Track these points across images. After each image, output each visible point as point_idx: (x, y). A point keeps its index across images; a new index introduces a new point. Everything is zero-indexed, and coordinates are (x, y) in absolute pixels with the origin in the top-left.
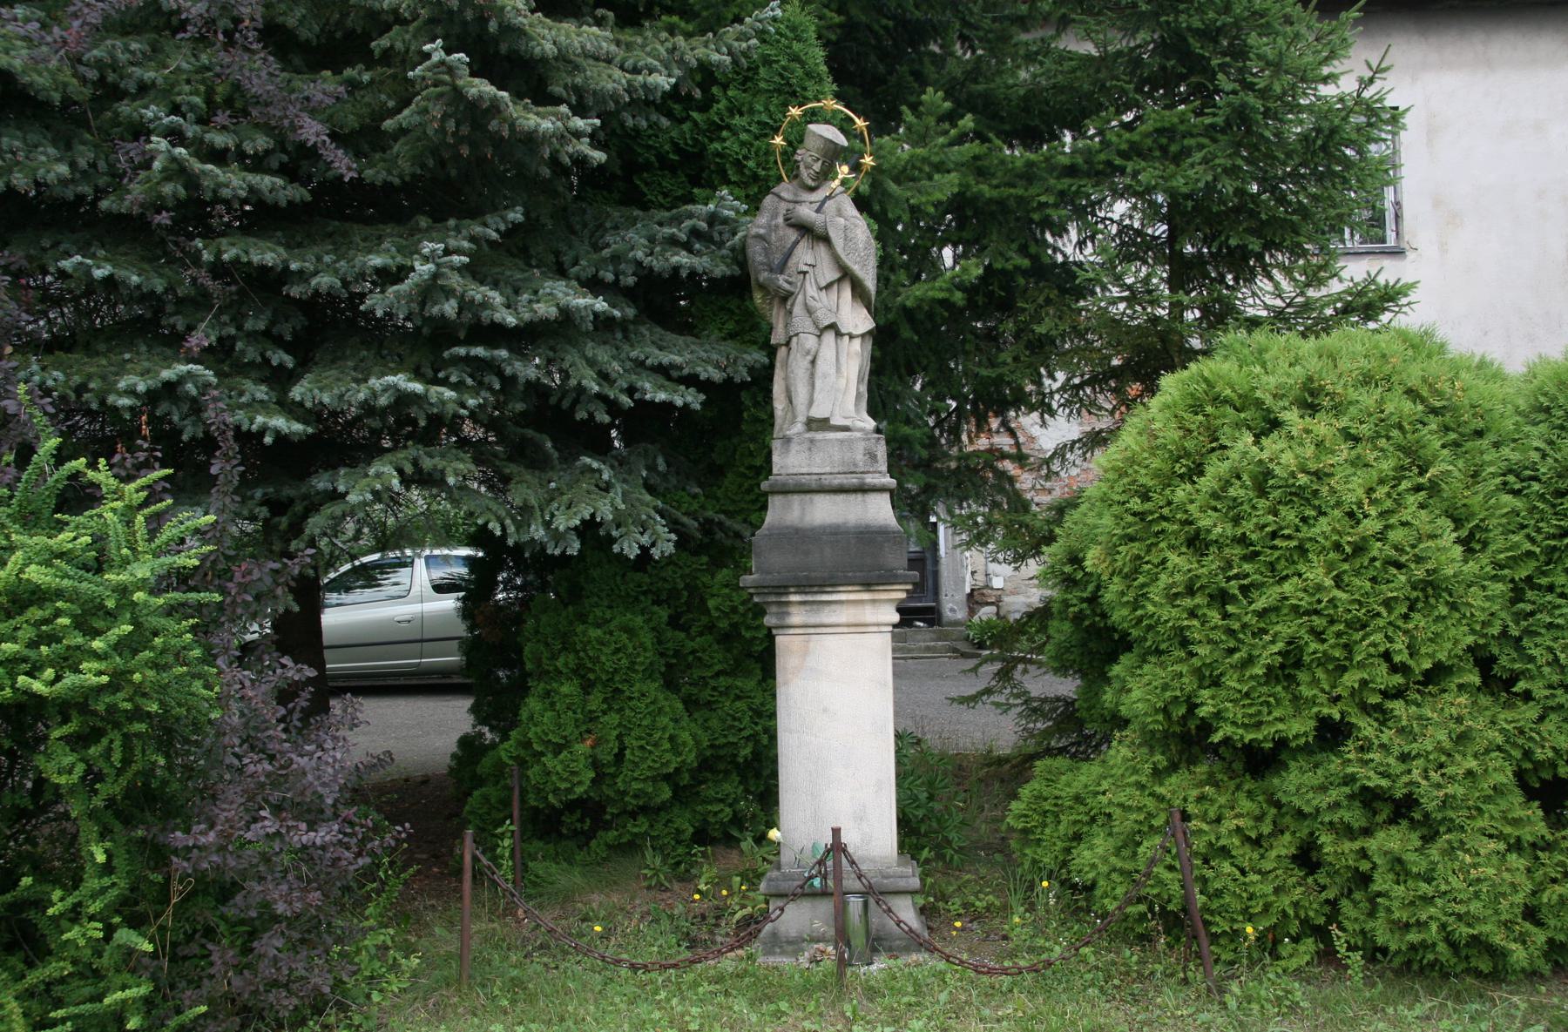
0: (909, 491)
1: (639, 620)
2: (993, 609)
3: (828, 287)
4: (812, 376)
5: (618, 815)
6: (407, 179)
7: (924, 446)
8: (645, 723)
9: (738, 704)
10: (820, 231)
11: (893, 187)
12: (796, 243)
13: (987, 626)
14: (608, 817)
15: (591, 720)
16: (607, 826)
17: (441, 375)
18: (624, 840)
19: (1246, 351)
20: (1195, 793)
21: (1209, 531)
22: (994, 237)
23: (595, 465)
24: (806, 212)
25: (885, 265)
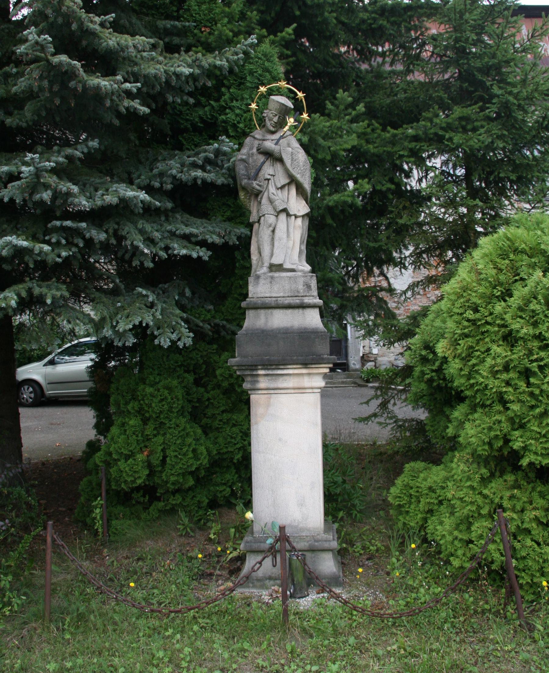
0: (332, 308)
1: (175, 382)
2: (373, 363)
3: (282, 187)
4: (273, 239)
5: (165, 493)
6: (31, 123)
7: (340, 284)
8: (178, 442)
9: (234, 429)
10: (277, 155)
11: (321, 141)
12: (264, 163)
13: (371, 372)
14: (158, 495)
15: (148, 440)
16: (159, 499)
17: (47, 238)
18: (168, 508)
19: (530, 223)
20: (508, 494)
21: (518, 331)
22: (376, 174)
23: (144, 292)
24: (269, 145)
25: (316, 183)
